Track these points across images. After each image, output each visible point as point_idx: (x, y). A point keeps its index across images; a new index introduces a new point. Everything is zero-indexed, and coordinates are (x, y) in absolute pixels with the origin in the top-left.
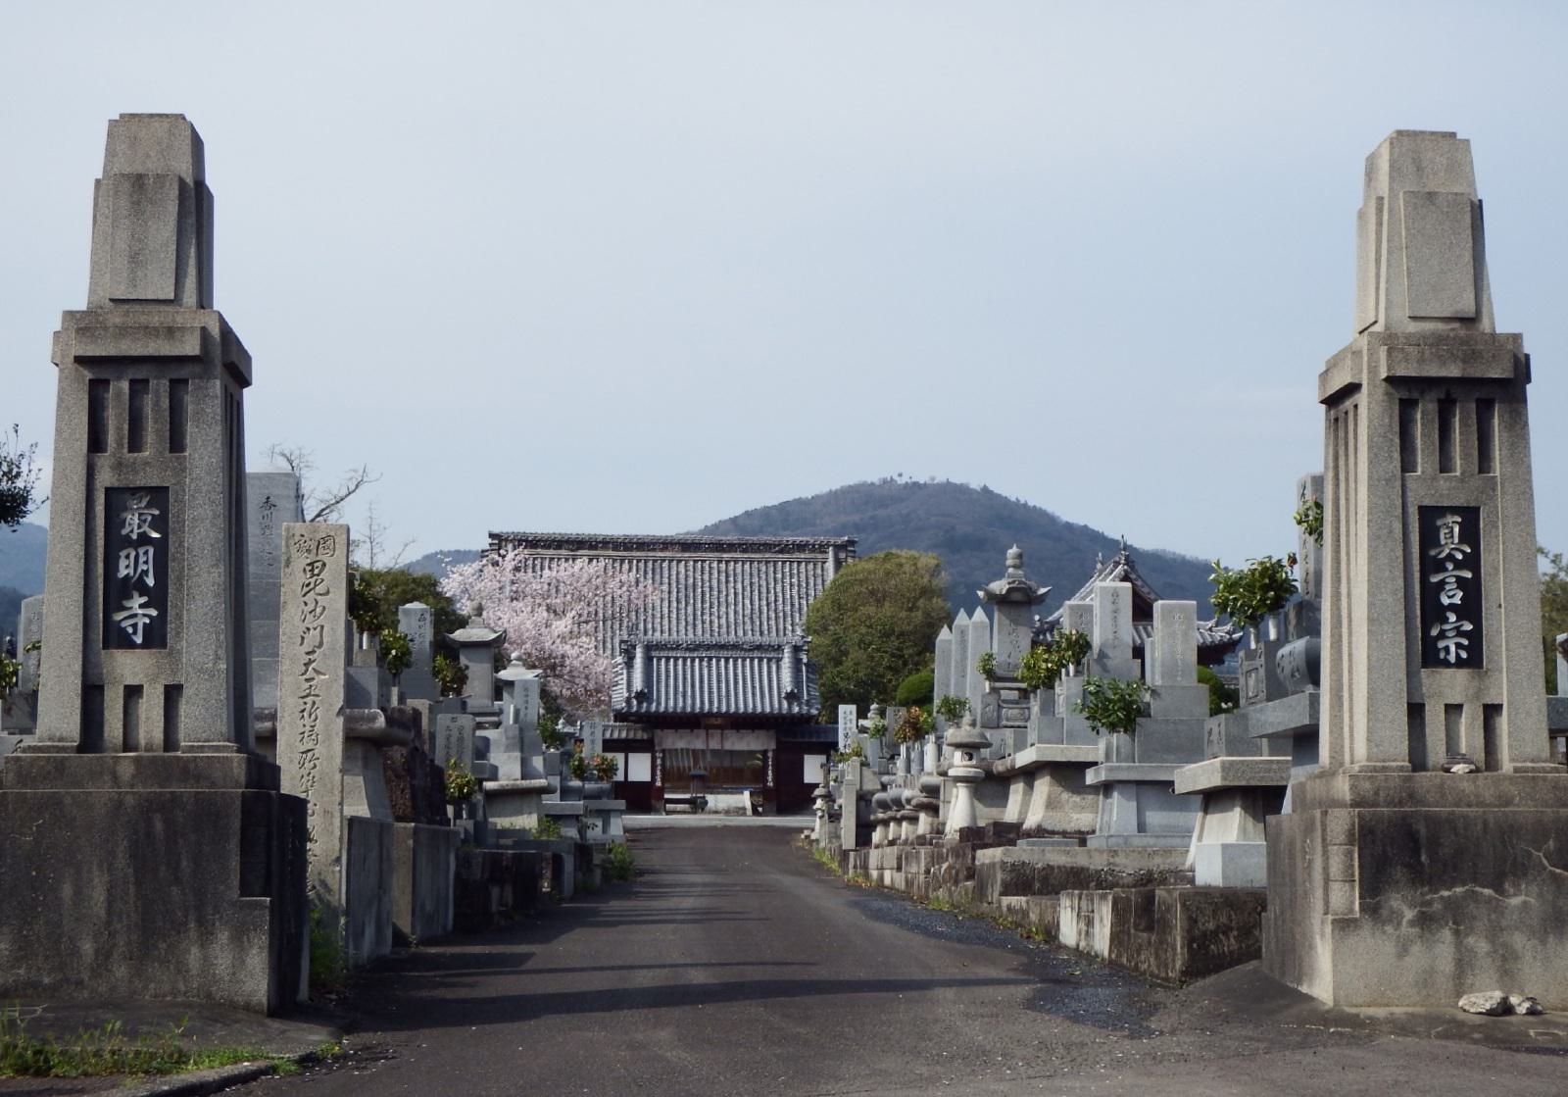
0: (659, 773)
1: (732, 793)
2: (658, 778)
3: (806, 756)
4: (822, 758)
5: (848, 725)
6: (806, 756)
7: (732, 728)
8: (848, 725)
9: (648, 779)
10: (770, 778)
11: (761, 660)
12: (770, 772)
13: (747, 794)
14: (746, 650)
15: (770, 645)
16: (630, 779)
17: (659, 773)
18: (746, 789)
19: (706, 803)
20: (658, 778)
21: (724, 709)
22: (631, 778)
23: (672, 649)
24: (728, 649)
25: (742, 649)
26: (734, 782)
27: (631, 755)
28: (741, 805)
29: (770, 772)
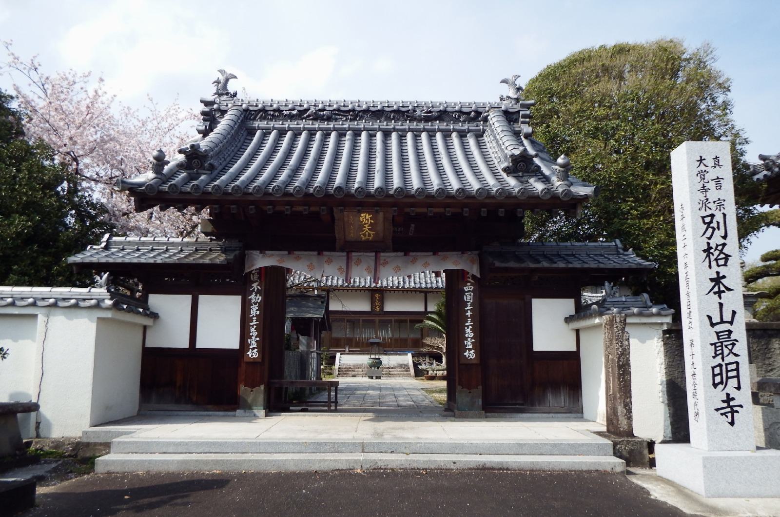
0: (254, 332)
1: (399, 355)
2: (253, 342)
3: (573, 300)
4: (567, 306)
5: (713, 195)
6: (573, 300)
7: (395, 250)
8: (713, 195)
9: (235, 344)
10: (469, 344)
11: (447, 135)
12: (469, 333)
13: (410, 355)
14: (419, 120)
15: (461, 112)
16: (200, 345)
17: (254, 332)
18: (409, 351)
19: (381, 363)
20: (253, 342)
21: (377, 182)
22: (202, 343)
23: (291, 117)
24: (388, 119)
25: (413, 119)
26: (401, 347)
27: (202, 298)
28: (405, 363)
29: (469, 333)
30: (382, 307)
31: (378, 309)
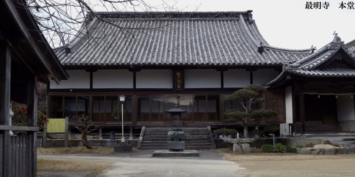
30: (183, 85)
31: (179, 87)
